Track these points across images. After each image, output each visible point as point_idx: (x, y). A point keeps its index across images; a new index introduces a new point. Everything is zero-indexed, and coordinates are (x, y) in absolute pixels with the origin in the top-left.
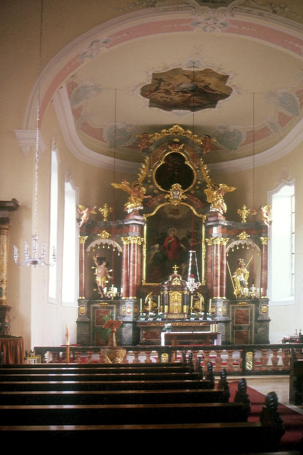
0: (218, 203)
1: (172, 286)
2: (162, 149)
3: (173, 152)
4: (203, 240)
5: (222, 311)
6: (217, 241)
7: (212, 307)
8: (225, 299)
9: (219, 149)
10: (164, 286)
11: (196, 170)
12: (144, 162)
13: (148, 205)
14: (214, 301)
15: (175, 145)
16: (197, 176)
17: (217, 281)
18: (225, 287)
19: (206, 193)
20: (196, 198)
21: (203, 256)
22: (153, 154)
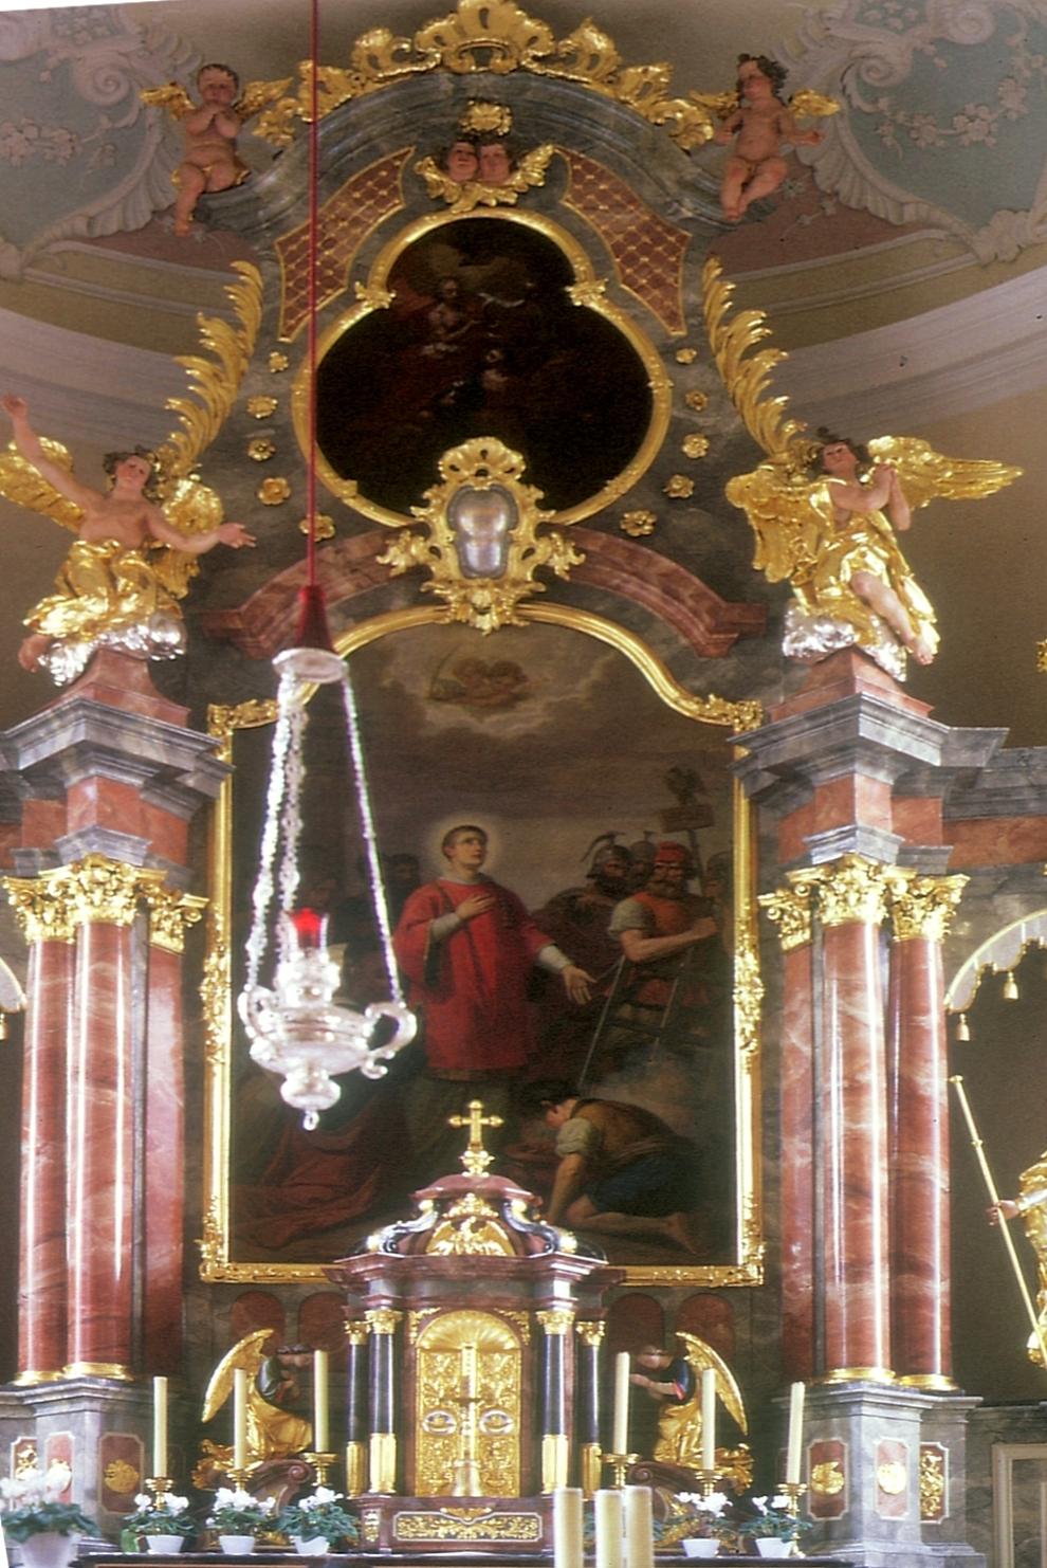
0: (846, 576)
1: (436, 1271)
2: (370, 194)
3: (461, 211)
4: (743, 907)
5: (914, 1485)
6: (853, 897)
7: (819, 1454)
8: (949, 1388)
9: (902, 229)
10: (360, 1269)
11: (668, 352)
12: (225, 312)
13: (239, 625)
14: (830, 1407)
15: (477, 155)
16: (679, 395)
17: (856, 1235)
18: (938, 1288)
19: (746, 507)
20: (667, 564)
21: (739, 1041)
22: (291, 241)
